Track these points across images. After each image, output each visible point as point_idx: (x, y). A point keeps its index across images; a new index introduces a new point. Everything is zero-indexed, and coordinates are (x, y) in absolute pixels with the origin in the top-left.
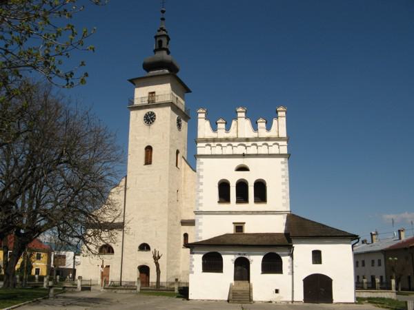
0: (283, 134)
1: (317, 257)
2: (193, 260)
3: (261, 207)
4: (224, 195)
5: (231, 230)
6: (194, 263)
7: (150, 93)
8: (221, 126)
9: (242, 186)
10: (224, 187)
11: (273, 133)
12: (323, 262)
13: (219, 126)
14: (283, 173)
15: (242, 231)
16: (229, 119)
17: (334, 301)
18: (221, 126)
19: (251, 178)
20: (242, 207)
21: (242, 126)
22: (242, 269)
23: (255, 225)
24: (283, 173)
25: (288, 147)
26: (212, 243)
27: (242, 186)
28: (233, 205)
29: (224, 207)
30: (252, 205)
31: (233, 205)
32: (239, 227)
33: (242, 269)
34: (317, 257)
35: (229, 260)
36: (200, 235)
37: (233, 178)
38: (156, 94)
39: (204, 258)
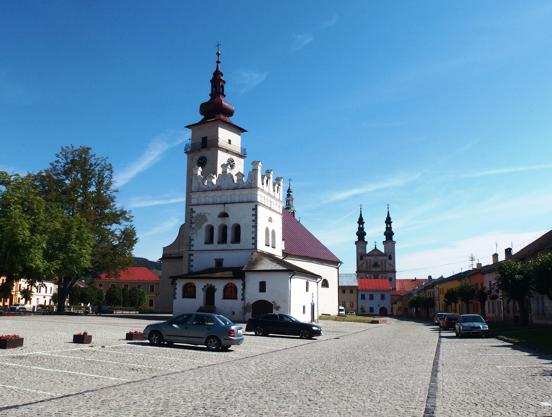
1: (263, 287)
4: (210, 240)
6: (176, 291)
7: (203, 138)
9: (224, 228)
10: (211, 229)
19: (230, 222)
20: (222, 246)
22: (210, 292)
27: (224, 228)
29: (209, 247)
30: (229, 245)
31: (215, 245)
32: (219, 262)
33: (210, 292)
34: (263, 287)
35: (200, 286)
36: (192, 269)
37: (217, 223)
38: (208, 139)
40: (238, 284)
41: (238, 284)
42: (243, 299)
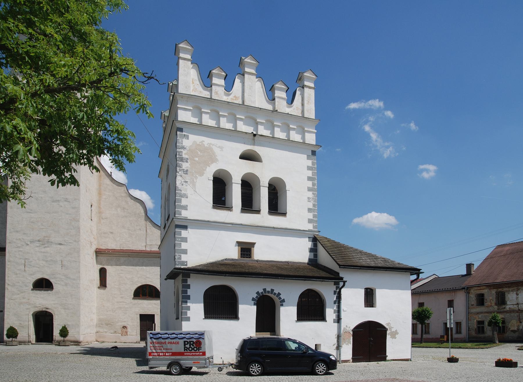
0: (310, 112)
1: (370, 299)
2: (189, 287)
3: (276, 221)
4: (220, 199)
5: (234, 253)
8: (218, 81)
9: (248, 187)
10: (220, 186)
11: (295, 109)
12: (240, 315)
13: (215, 80)
14: (184, 246)
15: (250, 257)
16: (233, 74)
17: (388, 358)
18: (218, 81)
19: (263, 174)
20: (249, 218)
21: (251, 90)
23: (270, 250)
24: (184, 246)
25: (317, 135)
26: (211, 269)
28: (235, 214)
29: (221, 215)
30: (264, 217)
32: (246, 250)
34: (370, 299)
35: (246, 292)
36: (184, 258)
39: (302, 296)
40: (326, 291)
41: (326, 291)
42: (338, 320)
